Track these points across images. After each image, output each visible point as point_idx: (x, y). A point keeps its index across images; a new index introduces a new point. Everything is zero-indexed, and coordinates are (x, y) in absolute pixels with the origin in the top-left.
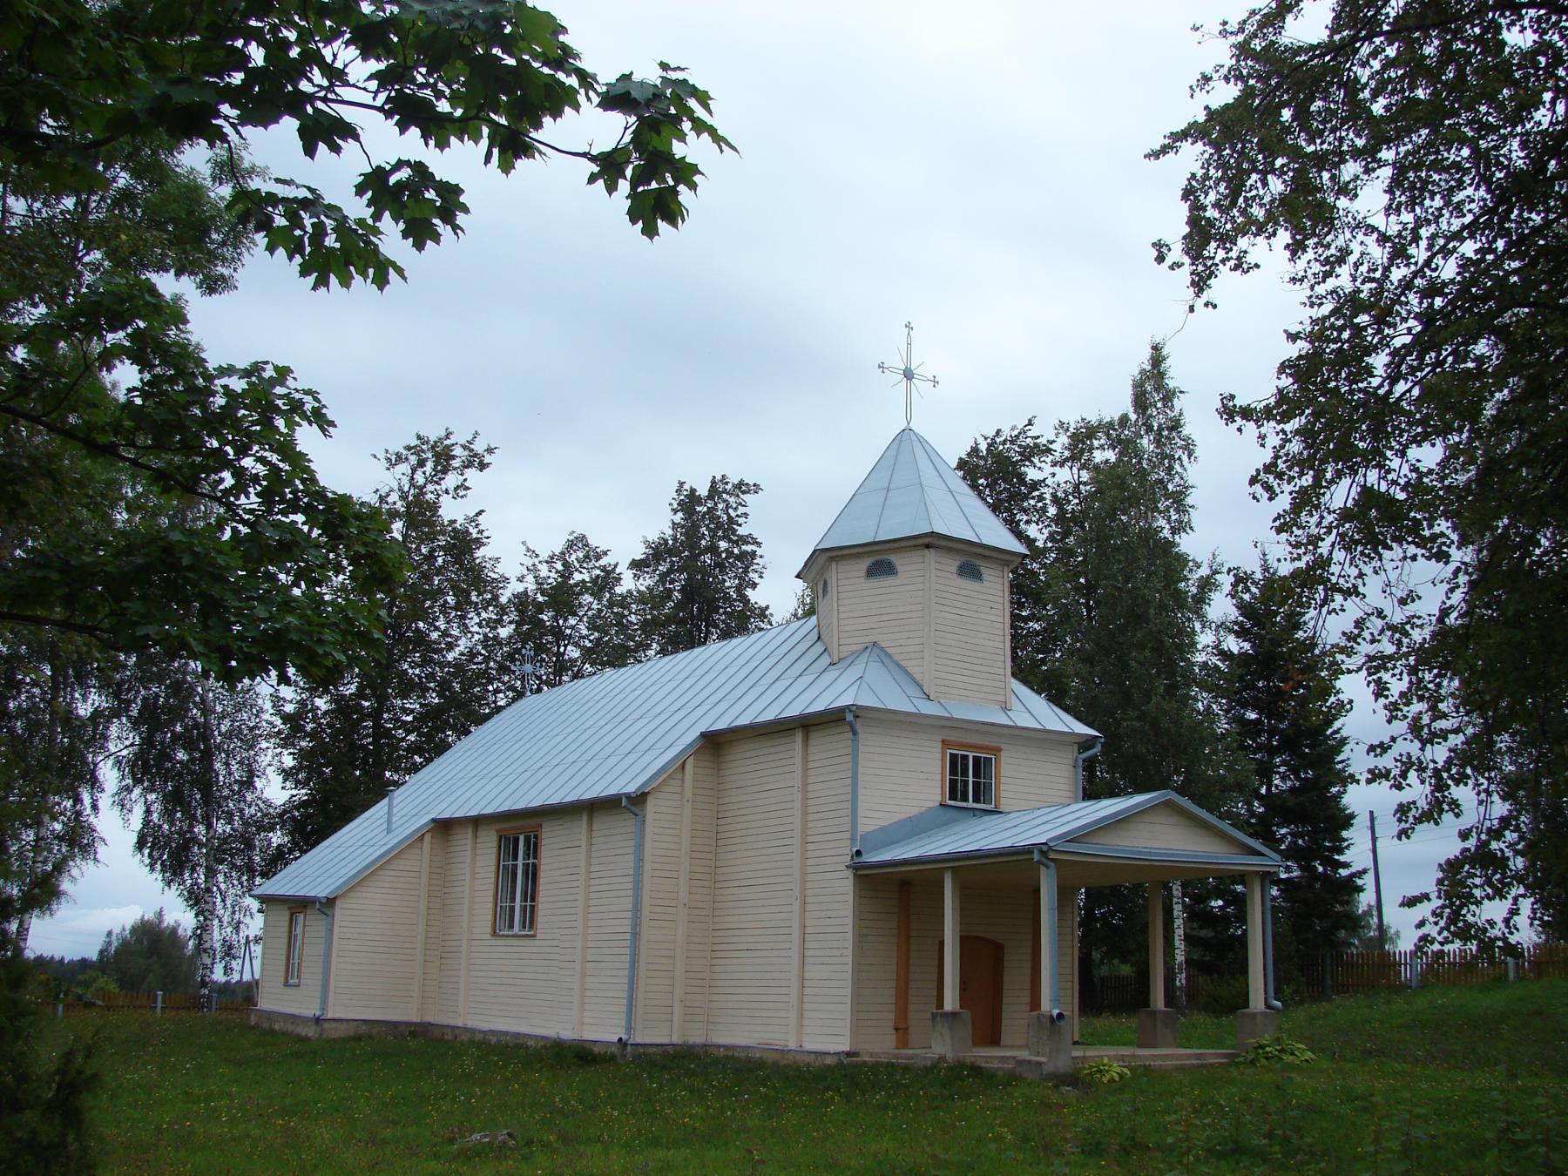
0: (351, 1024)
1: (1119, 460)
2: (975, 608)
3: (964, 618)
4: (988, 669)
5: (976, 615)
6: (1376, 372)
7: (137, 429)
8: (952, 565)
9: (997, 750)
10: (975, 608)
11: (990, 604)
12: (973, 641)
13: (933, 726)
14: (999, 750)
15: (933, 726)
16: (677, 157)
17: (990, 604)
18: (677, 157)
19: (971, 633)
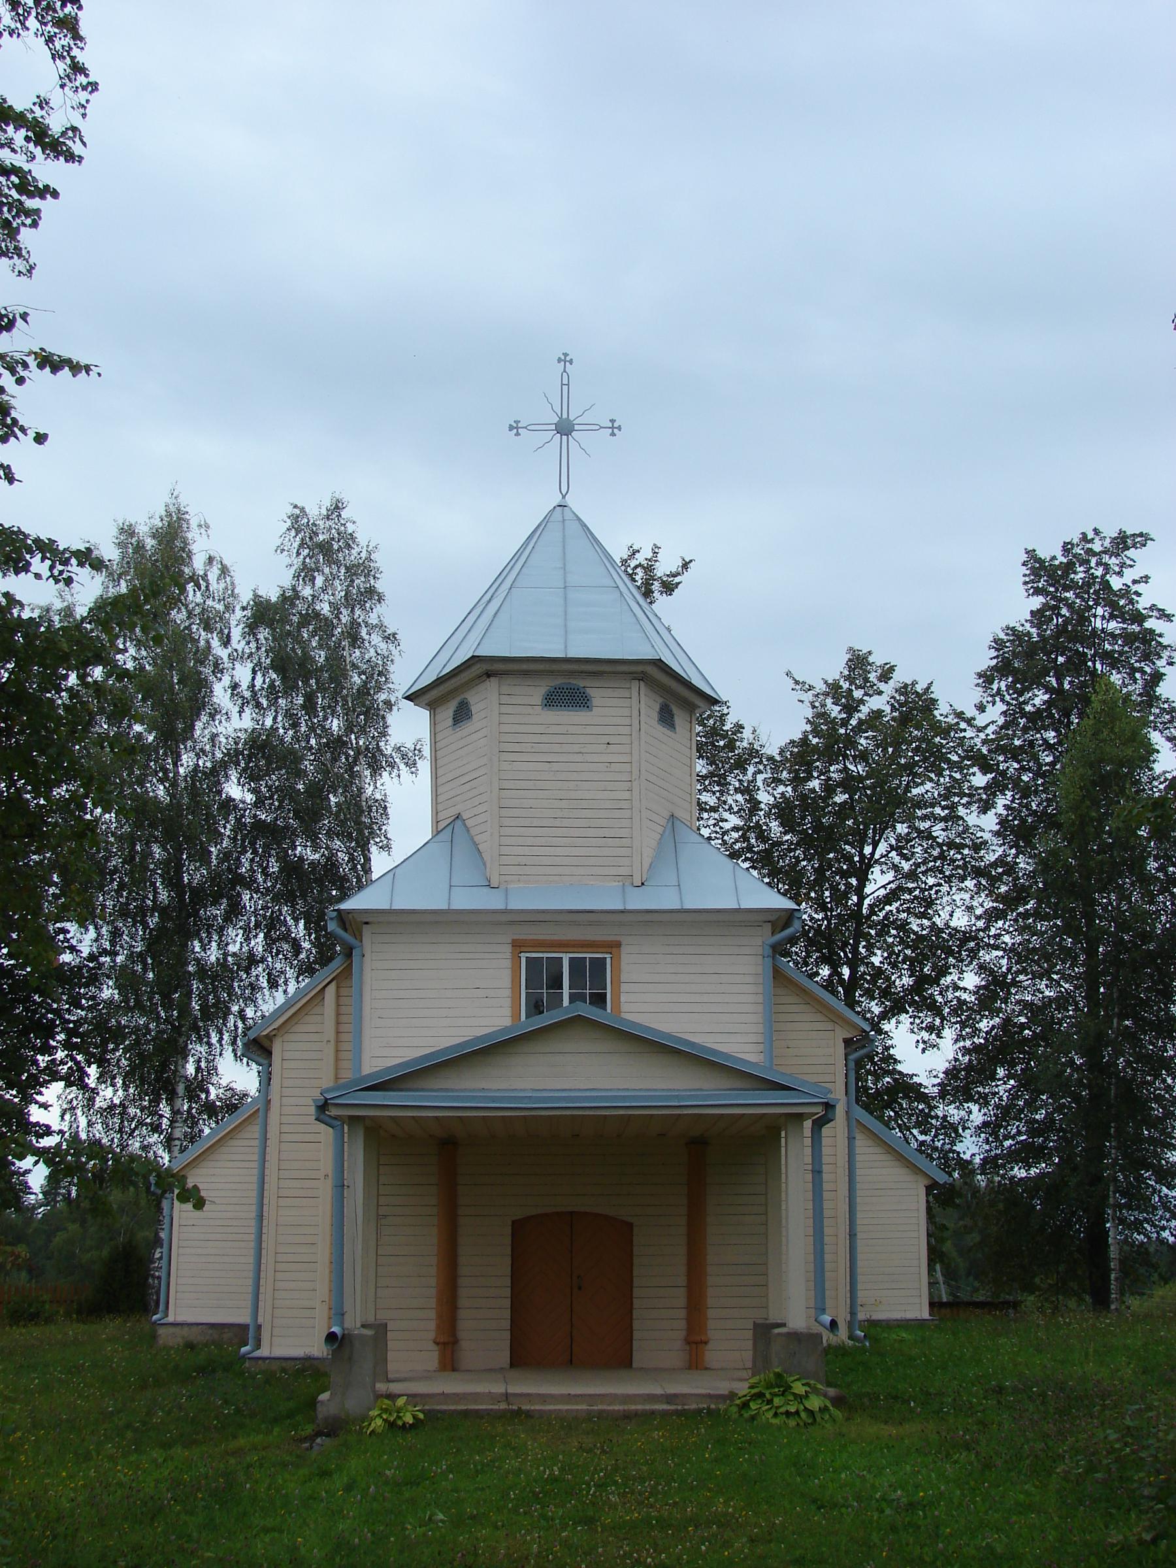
0: (194, 1329)
1: (1074, 867)
2: (576, 748)
3: (555, 766)
4: (601, 833)
5: (578, 758)
6: (220, 648)
7: (329, 648)
8: (536, 693)
9: (614, 946)
10: (576, 748)
11: (606, 739)
12: (573, 795)
13: (499, 923)
14: (618, 945)
15: (499, 923)
16: (274, 599)
17: (606, 739)
18: (274, 599)
19: (571, 785)
